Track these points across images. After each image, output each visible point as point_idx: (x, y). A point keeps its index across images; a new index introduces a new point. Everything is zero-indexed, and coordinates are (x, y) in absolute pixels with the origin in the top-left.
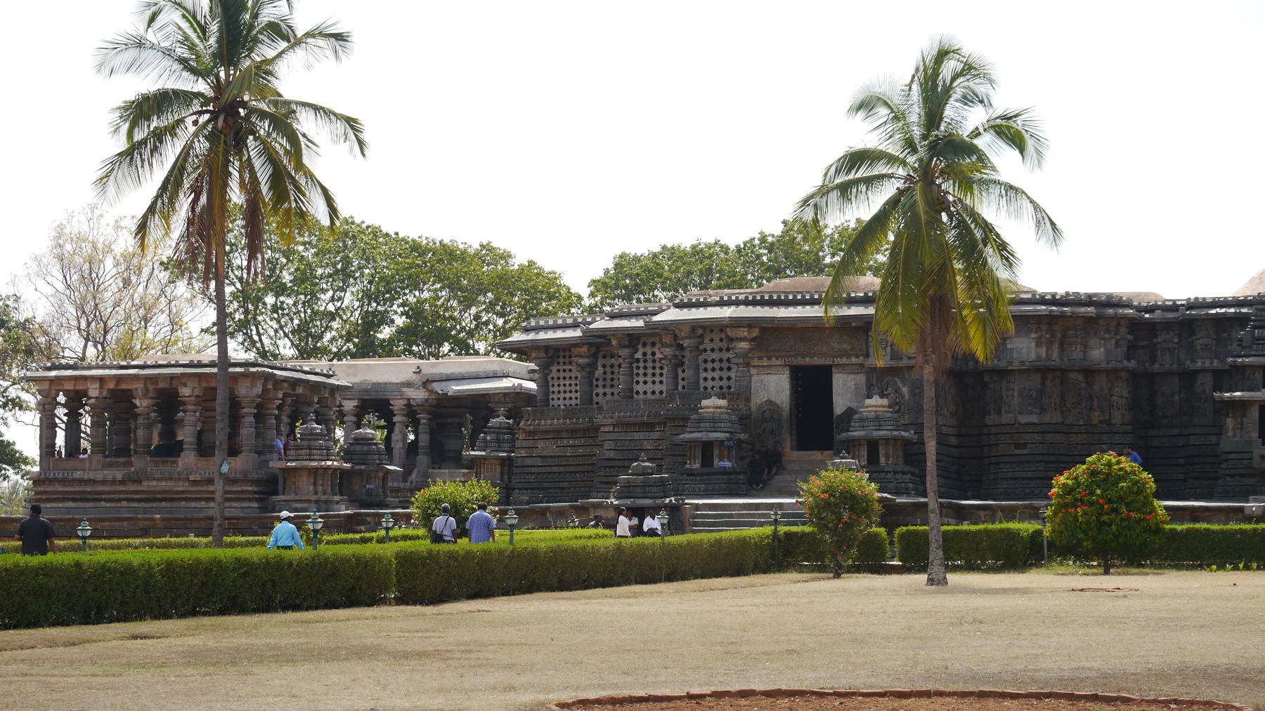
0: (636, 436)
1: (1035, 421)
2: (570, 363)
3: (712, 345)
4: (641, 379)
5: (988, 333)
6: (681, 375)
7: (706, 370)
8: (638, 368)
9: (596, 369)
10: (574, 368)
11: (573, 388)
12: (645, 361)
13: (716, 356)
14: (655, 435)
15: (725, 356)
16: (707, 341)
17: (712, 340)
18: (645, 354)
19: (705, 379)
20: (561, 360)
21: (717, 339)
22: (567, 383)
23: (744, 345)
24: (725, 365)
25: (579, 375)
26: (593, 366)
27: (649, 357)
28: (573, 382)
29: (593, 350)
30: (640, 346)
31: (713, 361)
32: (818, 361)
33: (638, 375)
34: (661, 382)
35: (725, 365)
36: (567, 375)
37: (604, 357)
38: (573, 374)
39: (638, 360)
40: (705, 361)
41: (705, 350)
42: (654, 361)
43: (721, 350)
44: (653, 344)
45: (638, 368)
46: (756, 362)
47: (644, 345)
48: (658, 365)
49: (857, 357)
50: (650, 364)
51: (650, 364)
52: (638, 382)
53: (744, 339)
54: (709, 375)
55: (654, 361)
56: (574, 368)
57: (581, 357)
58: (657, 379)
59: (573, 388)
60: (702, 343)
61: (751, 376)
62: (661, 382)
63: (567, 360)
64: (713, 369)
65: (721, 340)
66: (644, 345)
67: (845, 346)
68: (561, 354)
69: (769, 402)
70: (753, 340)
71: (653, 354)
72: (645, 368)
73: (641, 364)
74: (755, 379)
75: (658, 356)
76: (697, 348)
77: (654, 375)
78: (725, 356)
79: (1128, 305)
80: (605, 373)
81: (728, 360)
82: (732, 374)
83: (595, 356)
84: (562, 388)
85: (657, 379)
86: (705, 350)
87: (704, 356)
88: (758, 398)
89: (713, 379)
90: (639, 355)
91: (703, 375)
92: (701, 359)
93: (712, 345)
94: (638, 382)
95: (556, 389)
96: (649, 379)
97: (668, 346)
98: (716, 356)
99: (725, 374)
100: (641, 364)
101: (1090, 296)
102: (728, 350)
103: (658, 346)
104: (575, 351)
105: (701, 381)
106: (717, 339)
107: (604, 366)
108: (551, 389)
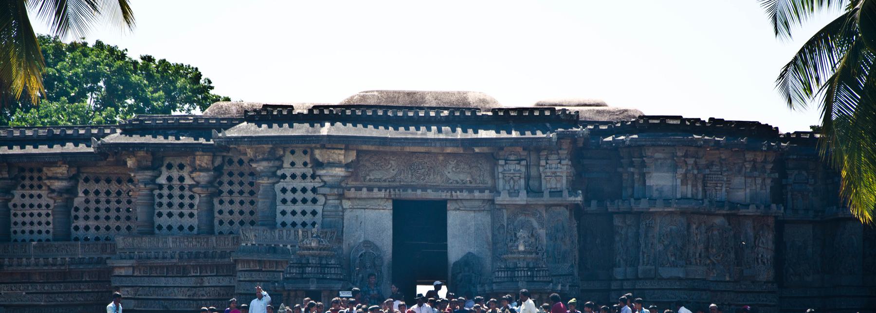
0: (163, 282)
1: (681, 275)
2: (40, 187)
3: (293, 170)
4: (165, 210)
5: (335, 146)
6: (217, 207)
7: (284, 201)
8: (161, 196)
9: (76, 195)
10: (44, 192)
11: (43, 219)
12: (170, 188)
13: (298, 184)
14: (192, 282)
15: (309, 184)
16: (286, 165)
17: (293, 164)
18: (170, 179)
19: (284, 213)
20: (27, 182)
21: (299, 164)
22: (35, 212)
23: (340, 172)
24: (309, 195)
25: (51, 202)
26: (71, 192)
27: (176, 182)
28: (44, 212)
29: (74, 171)
30: (164, 169)
31: (294, 190)
32: (431, 195)
33: (160, 204)
34: (191, 215)
35: (309, 195)
36: (36, 201)
37: (86, 180)
38: (43, 202)
39: (161, 187)
40: (284, 190)
41: (284, 176)
42: (182, 188)
43: (304, 176)
44: (181, 167)
45: (161, 196)
46: (352, 193)
47: (170, 167)
48: (187, 193)
49: (482, 191)
50: (176, 192)
51: (176, 192)
52: (160, 215)
53: (339, 165)
54: (289, 208)
55: (182, 188)
56: (44, 192)
57: (57, 179)
58: (186, 211)
59: (43, 219)
60: (280, 167)
61: (344, 210)
62: (191, 215)
63: (35, 183)
64: (294, 201)
65: (305, 164)
66: (170, 167)
67: (462, 176)
68: (28, 175)
69: (367, 243)
70: (347, 166)
71: (182, 179)
72: (170, 196)
73: (165, 192)
74: (348, 215)
75: (188, 181)
76: (274, 174)
77: (181, 205)
78: (309, 184)
79: (573, 119)
80: (87, 201)
81: (314, 190)
82: (319, 208)
83: (74, 178)
84: (27, 219)
85: (186, 211)
86: (284, 176)
87: (282, 184)
88: (354, 237)
89: (294, 213)
90: (162, 180)
91: (280, 207)
92: (278, 187)
93: (293, 170)
94: (160, 215)
95: (19, 219)
96: (175, 210)
97: (202, 169)
98: (298, 184)
99: (309, 207)
100: (165, 192)
101: (541, 108)
102: (313, 177)
103: (187, 169)
104: (47, 171)
105: (279, 216)
106: (299, 164)
107: (86, 192)
108: (13, 219)
